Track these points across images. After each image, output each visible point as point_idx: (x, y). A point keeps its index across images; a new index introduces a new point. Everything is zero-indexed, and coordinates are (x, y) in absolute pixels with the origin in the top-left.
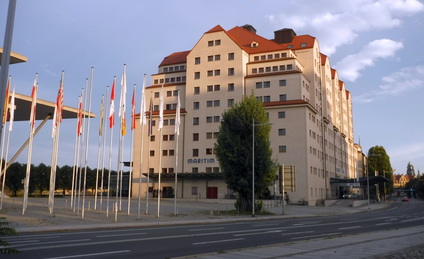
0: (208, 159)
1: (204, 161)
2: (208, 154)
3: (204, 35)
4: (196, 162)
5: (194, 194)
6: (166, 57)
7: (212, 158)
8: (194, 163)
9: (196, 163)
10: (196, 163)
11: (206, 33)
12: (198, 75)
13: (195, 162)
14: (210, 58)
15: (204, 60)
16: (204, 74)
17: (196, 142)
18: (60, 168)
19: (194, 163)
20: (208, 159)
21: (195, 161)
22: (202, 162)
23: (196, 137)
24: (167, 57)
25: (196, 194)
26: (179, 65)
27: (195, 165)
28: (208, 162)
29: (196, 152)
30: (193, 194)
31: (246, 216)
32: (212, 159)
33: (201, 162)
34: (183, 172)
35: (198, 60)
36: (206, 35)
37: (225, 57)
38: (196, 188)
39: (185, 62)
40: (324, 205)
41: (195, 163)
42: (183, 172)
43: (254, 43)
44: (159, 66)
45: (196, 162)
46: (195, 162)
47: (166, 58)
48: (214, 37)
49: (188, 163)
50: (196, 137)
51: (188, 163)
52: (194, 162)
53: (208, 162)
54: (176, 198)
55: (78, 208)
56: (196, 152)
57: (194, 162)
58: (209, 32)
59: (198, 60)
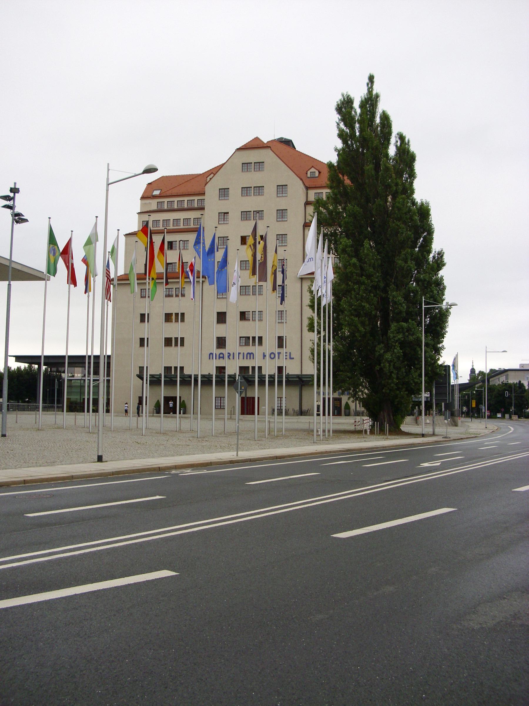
0: (244, 353)
1: (236, 356)
2: (168, 346)
3: (235, 152)
4: (223, 358)
5: (219, 407)
6: (150, 182)
7: (250, 352)
8: (219, 359)
9: (222, 359)
10: (223, 359)
11: (238, 149)
12: (282, 214)
13: (221, 357)
14: (246, 190)
15: (235, 192)
16: (234, 216)
17: (222, 326)
18: (440, 362)
19: (219, 359)
20: (244, 353)
21: (221, 357)
22: (233, 358)
23: (221, 317)
24: (152, 182)
25: (222, 407)
26: (196, 198)
27: (221, 363)
28: (243, 358)
29: (221, 342)
30: (217, 407)
31: (404, 437)
32: (250, 354)
33: (231, 357)
34: (301, 373)
35: (224, 193)
36: (238, 153)
37: (270, 190)
38: (222, 399)
39: (203, 194)
40: (417, 423)
41: (221, 359)
42: (301, 373)
43: (313, 170)
44: (141, 198)
45: (223, 358)
46: (221, 357)
47: (150, 185)
48: (253, 156)
49: (210, 359)
50: (221, 317)
51: (210, 359)
52: (220, 358)
53: (243, 358)
54: (193, 414)
55: (331, 421)
56: (221, 342)
57: (220, 358)
58: (243, 147)
59: (224, 193)
